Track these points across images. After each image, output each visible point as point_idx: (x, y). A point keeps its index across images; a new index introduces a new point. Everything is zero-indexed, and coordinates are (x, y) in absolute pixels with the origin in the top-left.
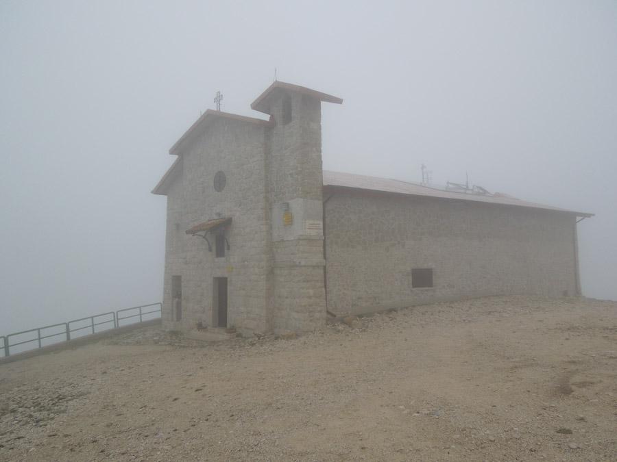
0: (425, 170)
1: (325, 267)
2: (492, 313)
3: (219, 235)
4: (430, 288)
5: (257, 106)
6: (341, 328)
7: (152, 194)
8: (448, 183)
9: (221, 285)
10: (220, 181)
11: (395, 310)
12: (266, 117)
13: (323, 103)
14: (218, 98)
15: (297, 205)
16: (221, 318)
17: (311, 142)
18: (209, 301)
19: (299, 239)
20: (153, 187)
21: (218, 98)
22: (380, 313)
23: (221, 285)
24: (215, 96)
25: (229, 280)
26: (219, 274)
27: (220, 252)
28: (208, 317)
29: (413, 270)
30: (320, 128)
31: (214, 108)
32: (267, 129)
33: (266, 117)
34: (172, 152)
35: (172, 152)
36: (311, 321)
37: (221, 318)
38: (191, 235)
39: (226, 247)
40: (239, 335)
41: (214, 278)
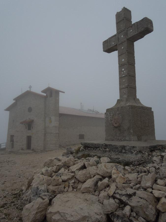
0: (82, 104)
1: (59, 134)
2: (153, 216)
3: (29, 125)
4: (83, 139)
5: (43, 92)
6: (63, 148)
7: (5, 111)
8: (88, 109)
9: (29, 139)
10: (30, 110)
11: (75, 145)
12: (45, 95)
13: (60, 93)
14: (30, 87)
15: (53, 118)
16: (29, 146)
17: (57, 102)
18: (25, 142)
19: (53, 127)
20: (5, 109)
21: (30, 87)
22: (72, 145)
23: (29, 139)
24: (29, 86)
25: (32, 136)
26: (28, 135)
27: (29, 129)
28: (25, 147)
29: (79, 135)
30: (59, 99)
31: (29, 89)
32: (46, 97)
33: (45, 95)
34: (14, 100)
35: (14, 100)
36: (56, 147)
37: (29, 146)
38: (21, 124)
39: (31, 128)
40: (35, 151)
41: (27, 136)
